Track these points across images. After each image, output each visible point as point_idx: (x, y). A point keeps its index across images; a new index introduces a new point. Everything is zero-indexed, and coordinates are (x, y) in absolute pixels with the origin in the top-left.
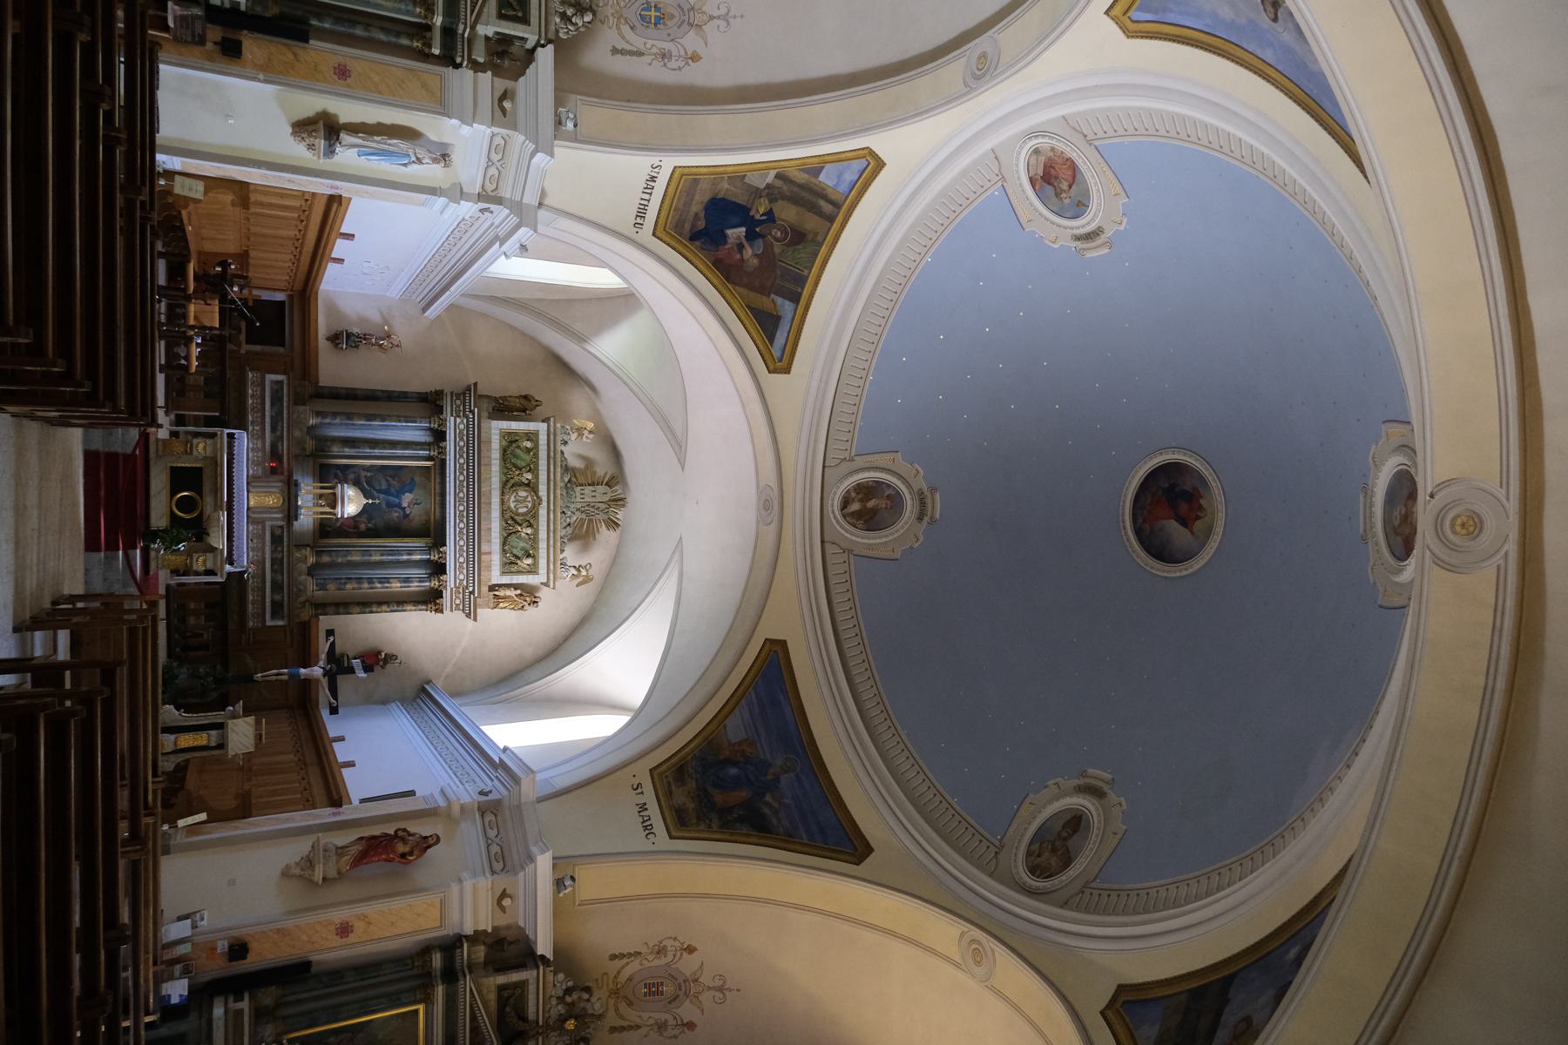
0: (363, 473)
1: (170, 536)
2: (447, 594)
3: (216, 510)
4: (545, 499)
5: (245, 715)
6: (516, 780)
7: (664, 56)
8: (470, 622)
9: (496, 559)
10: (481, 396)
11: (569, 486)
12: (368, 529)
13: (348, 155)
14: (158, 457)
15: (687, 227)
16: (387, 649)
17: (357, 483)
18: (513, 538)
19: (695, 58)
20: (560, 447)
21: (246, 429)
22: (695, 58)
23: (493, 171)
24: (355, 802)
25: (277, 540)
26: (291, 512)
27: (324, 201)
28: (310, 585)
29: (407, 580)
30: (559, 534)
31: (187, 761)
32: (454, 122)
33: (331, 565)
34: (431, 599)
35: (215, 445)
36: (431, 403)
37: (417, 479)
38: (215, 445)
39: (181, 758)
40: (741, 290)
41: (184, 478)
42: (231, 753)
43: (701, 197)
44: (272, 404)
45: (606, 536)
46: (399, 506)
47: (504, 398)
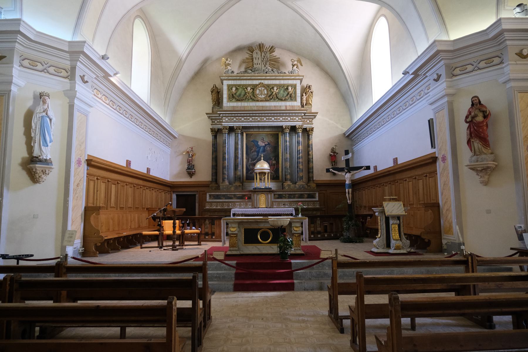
0: (250, 162)
1: (285, 246)
2: (305, 126)
3: (268, 222)
4: (260, 81)
5: (381, 206)
6: (438, 52)
8: (318, 116)
10: (213, 111)
11: (254, 70)
12: (275, 160)
13: (51, 150)
14: (239, 250)
16: (329, 152)
17: (254, 165)
18: (280, 96)
20: (235, 74)
21: (231, 209)
24: (433, 150)
25: (280, 197)
26: (268, 191)
28: (300, 183)
29: (298, 143)
30: (277, 74)
31: (405, 234)
32: (14, 88)
33: (291, 174)
34: (307, 132)
35: (231, 223)
36: (216, 133)
37: (252, 140)
38: (231, 223)
39: (404, 237)
41: (251, 236)
42: (404, 213)
44: (220, 199)
45: (277, 53)
46: (264, 147)
47: (213, 101)
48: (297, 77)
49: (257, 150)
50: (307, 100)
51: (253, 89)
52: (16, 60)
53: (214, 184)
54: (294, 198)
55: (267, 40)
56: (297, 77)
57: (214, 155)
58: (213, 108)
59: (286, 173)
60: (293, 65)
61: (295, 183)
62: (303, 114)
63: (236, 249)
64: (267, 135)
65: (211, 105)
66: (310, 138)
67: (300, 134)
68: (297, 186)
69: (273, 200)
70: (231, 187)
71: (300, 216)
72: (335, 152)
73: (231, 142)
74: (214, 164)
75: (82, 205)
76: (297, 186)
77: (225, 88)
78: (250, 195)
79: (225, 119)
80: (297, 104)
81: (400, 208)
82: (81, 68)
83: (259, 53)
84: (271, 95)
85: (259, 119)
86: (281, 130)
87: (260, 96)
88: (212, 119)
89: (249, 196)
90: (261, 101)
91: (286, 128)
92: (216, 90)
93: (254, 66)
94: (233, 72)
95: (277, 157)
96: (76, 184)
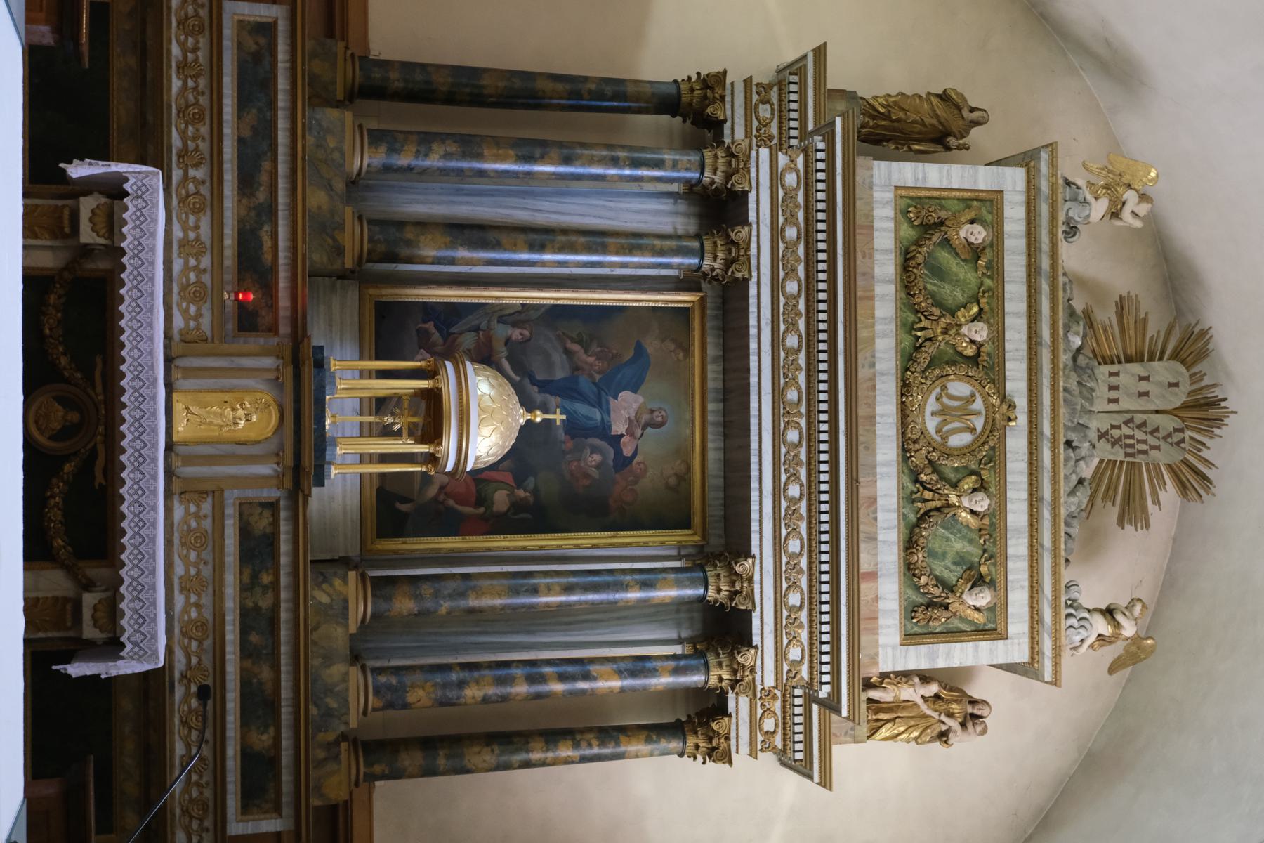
0: (501, 332)
2: (739, 704)
4: (1022, 402)
9: (887, 594)
10: (832, 92)
12: (517, 506)
17: (485, 358)
18: (934, 534)
21: (149, 150)
25: (257, 550)
26: (303, 453)
28: (355, 694)
29: (639, 666)
34: (697, 722)
36: (695, 109)
37: (652, 346)
46: (603, 432)
47: (900, 102)
48: (1047, 645)
49: (584, 384)
51: (974, 360)
53: (342, 77)
54: (247, 651)
56: (1047, 645)
57: (548, 86)
58: (851, 96)
59: (426, 589)
60: (1109, 613)
61: (355, 658)
62: (824, 691)
64: (683, 453)
65: (865, 92)
66: (663, 744)
67: (697, 679)
68: (337, 669)
69: (232, 497)
70: (329, 187)
73: (635, 204)
74: (486, 81)
77: (980, 178)
78: (273, 329)
79: (792, 167)
80: (889, 649)
83: (1178, 398)
84: (942, 478)
86: (716, 542)
87: (932, 405)
88: (781, 84)
89: (265, 318)
92: (956, 125)
93: (1105, 369)
94: (1072, 231)
95: (534, 517)
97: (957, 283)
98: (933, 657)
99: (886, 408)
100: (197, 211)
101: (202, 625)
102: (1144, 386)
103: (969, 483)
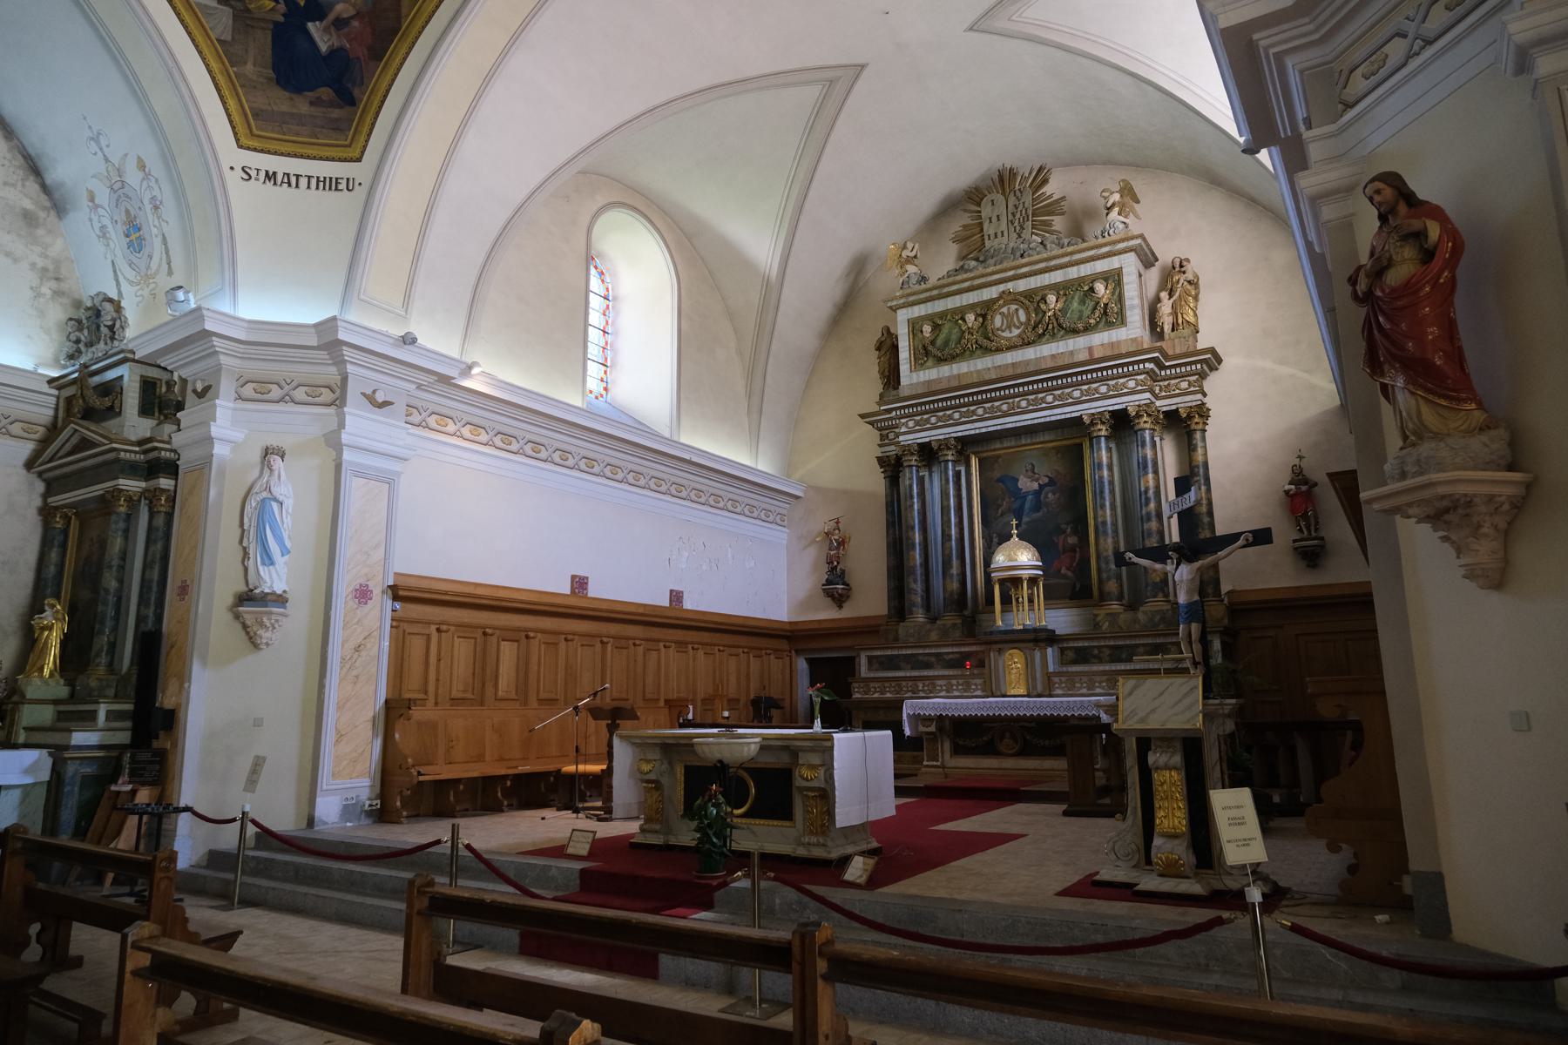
2: (1164, 405)
4: (1002, 287)
7: (156, 208)
8: (1229, 362)
9: (1100, 339)
12: (1075, 532)
15: (336, 113)
19: (142, 166)
20: (933, 281)
22: (142, 166)
23: (300, 394)
25: (1083, 656)
26: (1040, 638)
27: (398, 606)
32: (219, 450)
34: (1184, 426)
36: (892, 467)
37: (997, 474)
40: (404, 11)
43: (281, 101)
44: (898, 668)
46: (1037, 493)
49: (1016, 505)
50: (1175, 313)
51: (984, 316)
52: (226, 387)
55: (1017, 151)
59: (1104, 576)
63: (657, 827)
68: (1141, 616)
71: (818, 723)
72: (1306, 481)
75: (376, 693)
76: (1141, 616)
79: (906, 424)
81: (1187, 701)
82: (360, 377)
83: (1000, 198)
85: (1005, 407)
87: (1006, 334)
90: (1012, 347)
91: (1092, 424)
93: (988, 243)
96: (352, 644)
97: (950, 333)
98: (1133, 307)
99: (1009, 358)
100: (934, 686)
101: (1108, 681)
102: (994, 219)
103: (1043, 306)
